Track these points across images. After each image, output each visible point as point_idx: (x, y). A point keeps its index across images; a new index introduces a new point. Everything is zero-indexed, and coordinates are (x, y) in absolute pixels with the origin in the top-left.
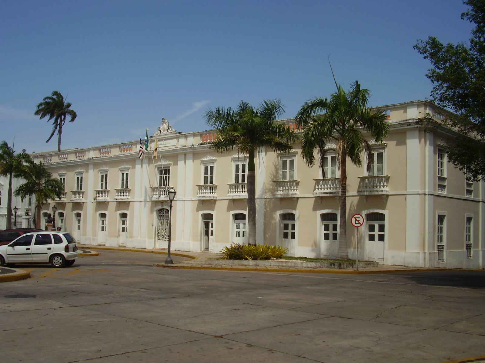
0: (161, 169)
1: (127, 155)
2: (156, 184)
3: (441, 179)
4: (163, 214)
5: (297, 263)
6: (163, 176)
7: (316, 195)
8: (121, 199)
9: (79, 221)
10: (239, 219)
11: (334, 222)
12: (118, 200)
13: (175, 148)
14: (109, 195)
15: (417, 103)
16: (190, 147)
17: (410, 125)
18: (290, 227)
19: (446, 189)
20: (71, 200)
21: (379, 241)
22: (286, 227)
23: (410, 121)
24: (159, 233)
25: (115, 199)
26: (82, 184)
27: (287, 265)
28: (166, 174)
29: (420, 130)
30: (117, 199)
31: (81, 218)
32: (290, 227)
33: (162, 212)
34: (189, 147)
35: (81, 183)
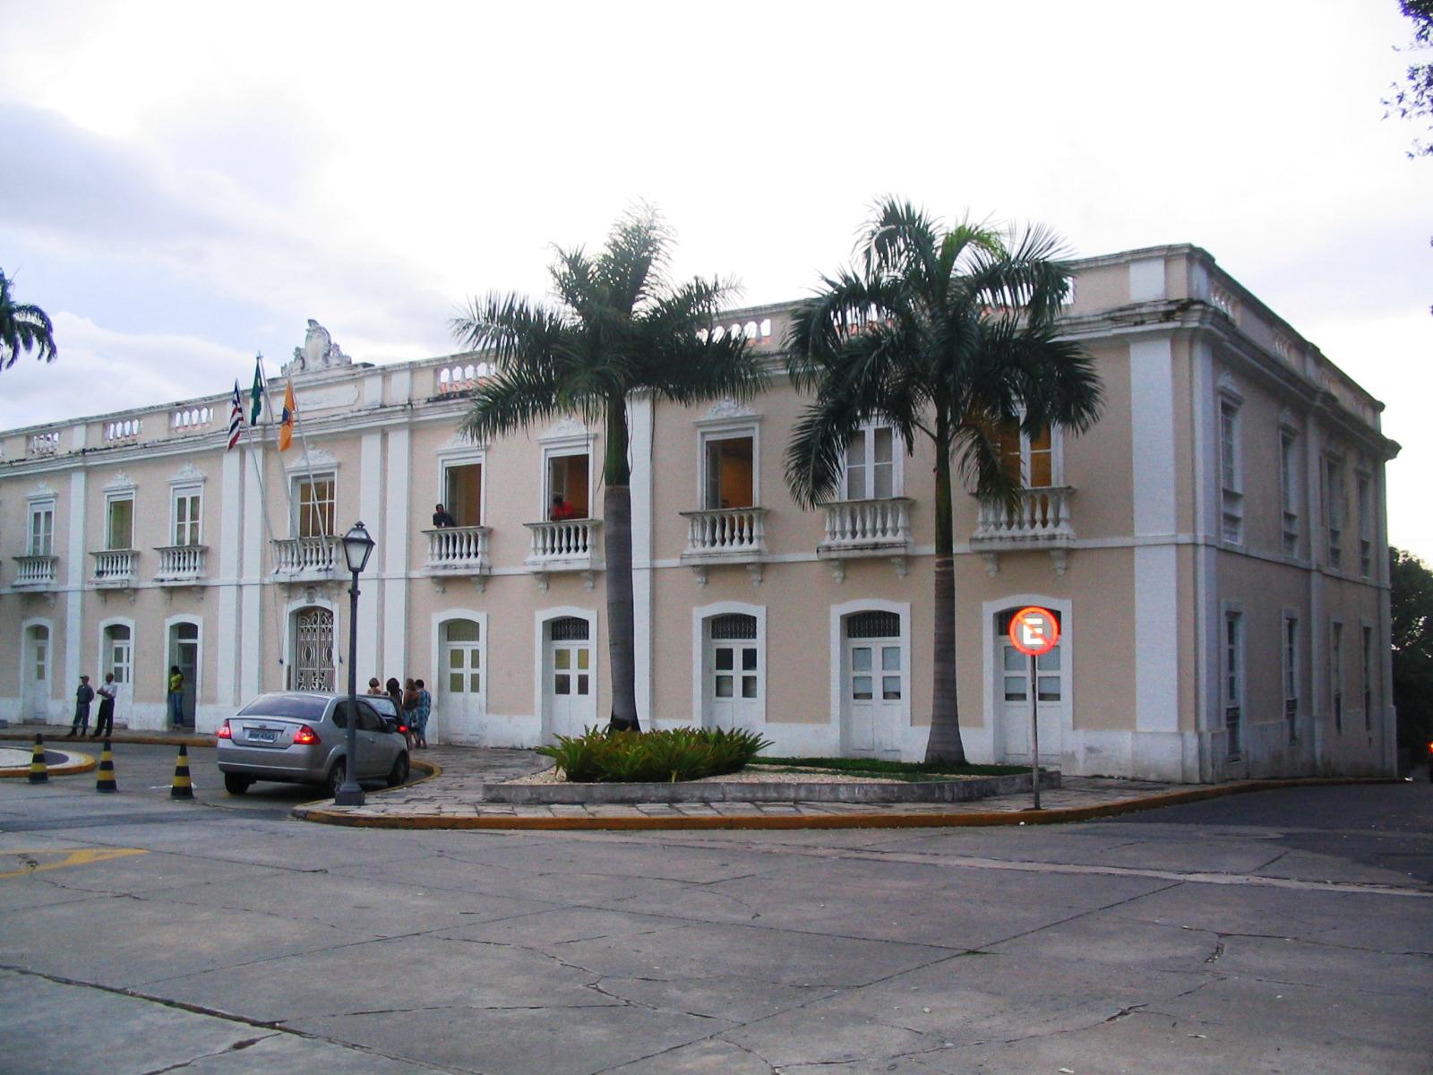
0: (305, 481)
1: (196, 438)
2: (286, 528)
3: (1230, 496)
4: (314, 626)
5: (817, 788)
6: (311, 503)
7: (827, 553)
8: (176, 580)
9: (41, 655)
10: (561, 635)
11: (747, 643)
12: (166, 584)
13: (352, 412)
14: (55, 572)
15: (1164, 253)
16: (401, 408)
17: (1143, 323)
18: (738, 660)
19: (1241, 530)
20: (15, 587)
21: (587, 693)
22: (724, 659)
23: (1144, 310)
24: (300, 684)
25: (157, 580)
26: (35, 533)
27: (783, 796)
28: (321, 496)
29: (1174, 336)
30: (162, 581)
31: (47, 644)
32: (738, 660)
33: (309, 617)
34: (398, 408)
35: (192, 519)
